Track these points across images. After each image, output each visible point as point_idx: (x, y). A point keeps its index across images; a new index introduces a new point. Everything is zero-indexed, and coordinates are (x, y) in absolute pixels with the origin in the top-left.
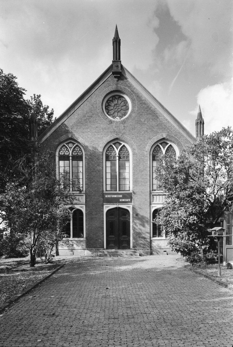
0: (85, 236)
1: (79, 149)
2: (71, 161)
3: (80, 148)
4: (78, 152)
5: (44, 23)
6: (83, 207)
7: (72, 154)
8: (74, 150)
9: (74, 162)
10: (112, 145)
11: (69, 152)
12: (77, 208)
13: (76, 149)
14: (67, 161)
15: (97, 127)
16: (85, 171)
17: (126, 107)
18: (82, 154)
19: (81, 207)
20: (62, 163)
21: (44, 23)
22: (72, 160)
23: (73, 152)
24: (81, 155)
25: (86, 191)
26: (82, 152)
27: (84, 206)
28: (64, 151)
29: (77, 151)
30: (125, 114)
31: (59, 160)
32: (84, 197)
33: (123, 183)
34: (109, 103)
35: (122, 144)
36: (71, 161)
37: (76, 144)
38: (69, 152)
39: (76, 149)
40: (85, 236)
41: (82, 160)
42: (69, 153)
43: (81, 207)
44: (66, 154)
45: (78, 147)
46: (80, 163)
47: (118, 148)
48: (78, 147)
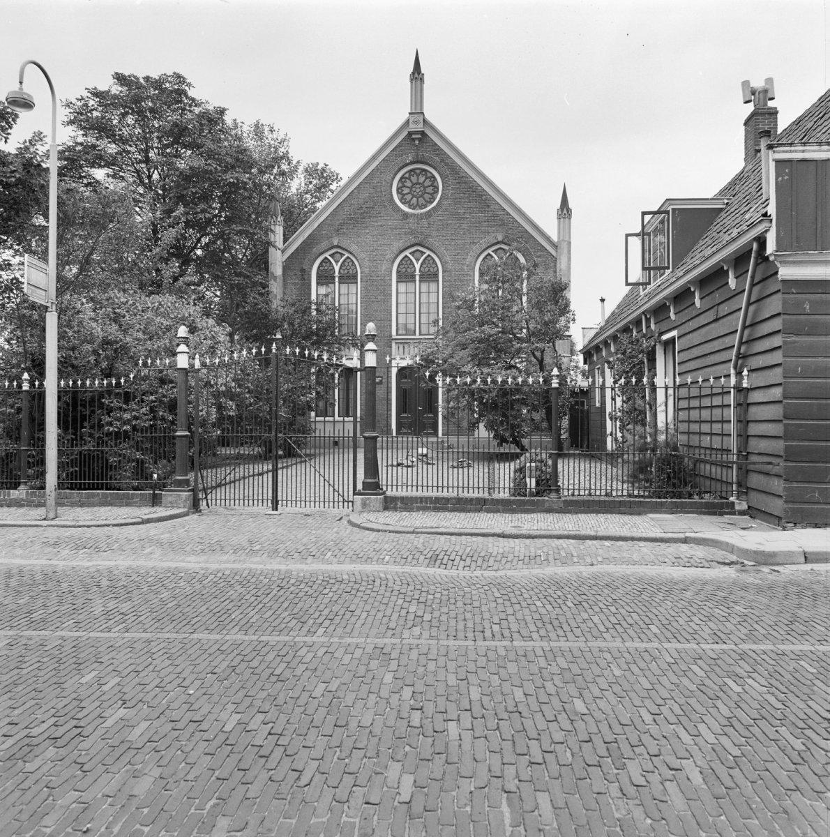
7: (420, 271)
18: (438, 270)
23: (340, 268)
28: (406, 266)
46: (353, 288)
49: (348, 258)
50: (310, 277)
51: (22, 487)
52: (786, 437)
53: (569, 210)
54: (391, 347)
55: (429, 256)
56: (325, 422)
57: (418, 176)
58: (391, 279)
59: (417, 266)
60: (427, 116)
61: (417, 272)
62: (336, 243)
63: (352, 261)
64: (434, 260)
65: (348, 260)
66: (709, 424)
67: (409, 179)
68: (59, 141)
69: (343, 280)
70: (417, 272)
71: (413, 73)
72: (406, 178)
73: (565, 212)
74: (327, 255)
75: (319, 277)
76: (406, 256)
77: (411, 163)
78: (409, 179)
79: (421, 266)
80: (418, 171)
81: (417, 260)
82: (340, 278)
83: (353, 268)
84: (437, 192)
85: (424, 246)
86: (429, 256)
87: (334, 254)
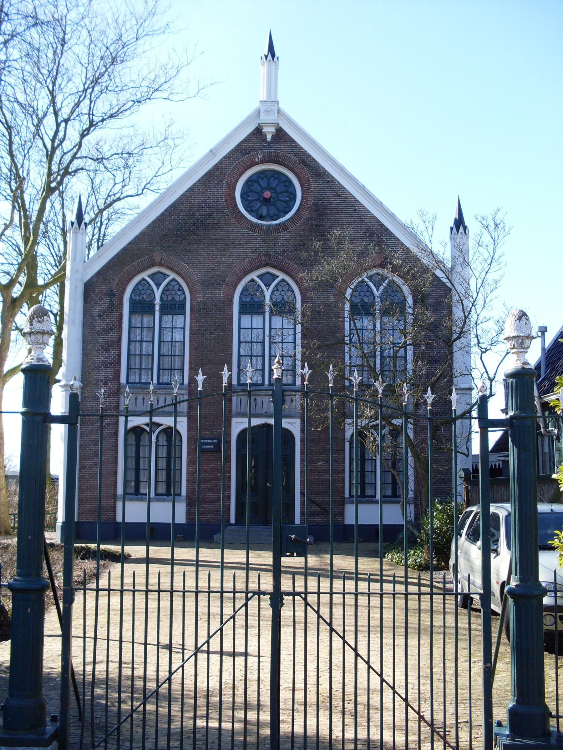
2: (157, 314)
7: (161, 299)
9: (168, 318)
10: (366, 280)
12: (166, 425)
14: (179, 316)
16: (190, 339)
17: (286, 206)
18: (185, 298)
19: (290, 423)
20: (246, 321)
22: (272, 314)
24: (181, 300)
26: (184, 293)
27: (298, 421)
30: (275, 217)
33: (143, 360)
35: (278, 277)
36: (157, 314)
41: (184, 313)
42: (185, 296)
43: (290, 423)
45: (176, 283)
46: (179, 320)
51: (555, 742)
52: (368, 741)
55: (283, 280)
56: (172, 562)
58: (232, 309)
59: (268, 294)
61: (157, 301)
64: (289, 286)
66: (143, 642)
68: (38, 188)
69: (165, 310)
70: (157, 301)
75: (133, 303)
76: (144, 280)
79: (272, 293)
82: (162, 307)
83: (179, 293)
84: (287, 213)
85: (169, 268)
86: (283, 280)
87: (154, 274)
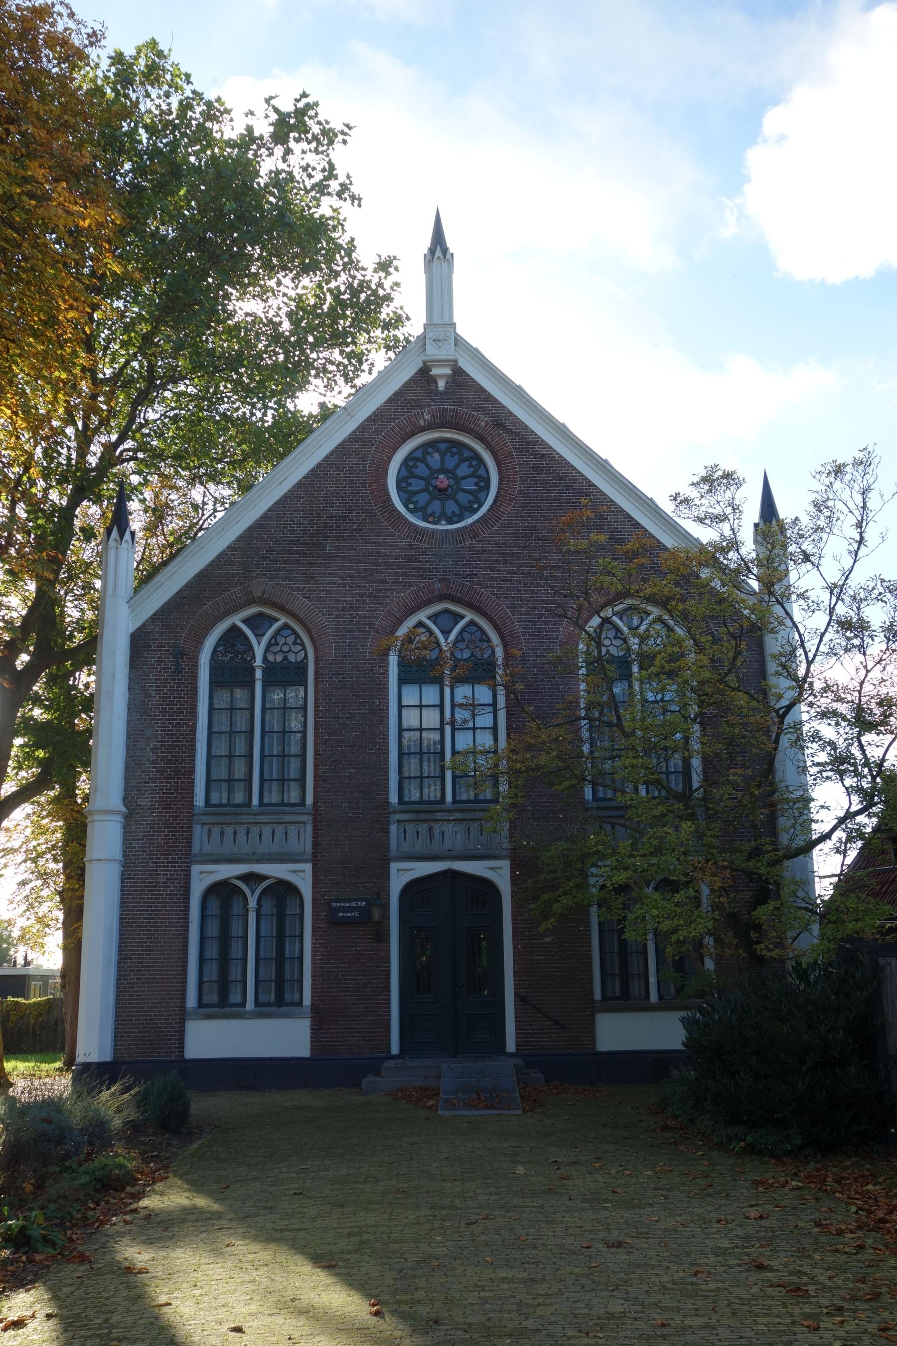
0: (307, 1000)
1: (291, 639)
3: (297, 636)
4: (290, 650)
5: (203, 188)
6: (501, 868)
7: (265, 659)
8: (273, 641)
11: (438, 649)
12: (276, 878)
13: (281, 641)
15: (363, 556)
18: (306, 657)
19: (492, 869)
20: (411, 695)
21: (203, 188)
23: (267, 650)
24: (298, 660)
25: (315, 802)
26: (304, 649)
28: (285, 648)
29: (285, 648)
31: (402, 681)
32: (309, 828)
34: (413, 470)
37: (283, 620)
38: (438, 649)
39: (281, 641)
40: (307, 1000)
42: (306, 654)
43: (492, 869)
44: (292, 658)
47: (263, 635)
48: (290, 632)
49: (286, 626)
50: (195, 668)
53: (445, 250)
54: (387, 831)
57: (462, 460)
60: (459, 331)
61: (258, 662)
62: (258, 593)
63: (295, 632)
65: (286, 632)
67: (424, 461)
70: (258, 662)
71: (432, 251)
72: (418, 460)
73: (438, 253)
74: (237, 619)
75: (403, 665)
77: (430, 427)
78: (424, 461)
80: (443, 446)
81: (446, 633)
86: (472, 623)
